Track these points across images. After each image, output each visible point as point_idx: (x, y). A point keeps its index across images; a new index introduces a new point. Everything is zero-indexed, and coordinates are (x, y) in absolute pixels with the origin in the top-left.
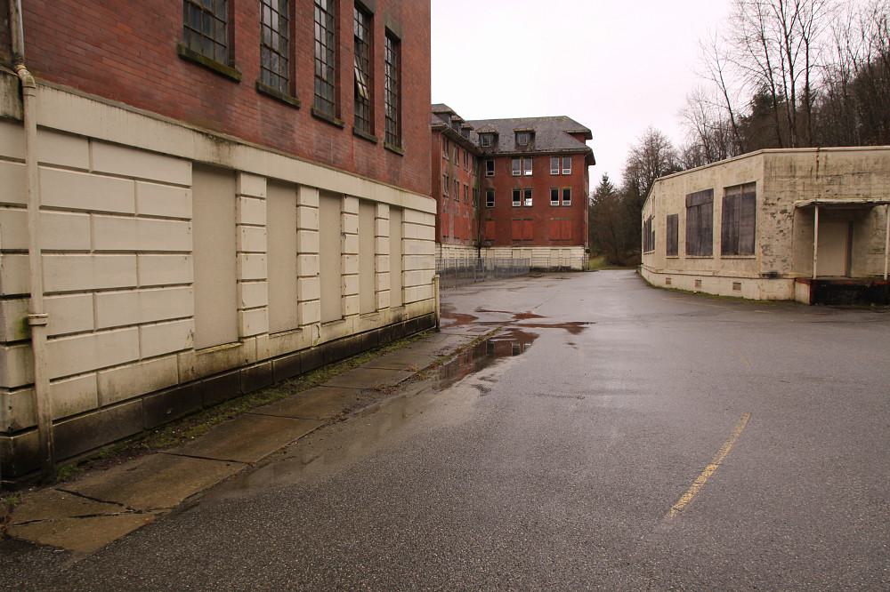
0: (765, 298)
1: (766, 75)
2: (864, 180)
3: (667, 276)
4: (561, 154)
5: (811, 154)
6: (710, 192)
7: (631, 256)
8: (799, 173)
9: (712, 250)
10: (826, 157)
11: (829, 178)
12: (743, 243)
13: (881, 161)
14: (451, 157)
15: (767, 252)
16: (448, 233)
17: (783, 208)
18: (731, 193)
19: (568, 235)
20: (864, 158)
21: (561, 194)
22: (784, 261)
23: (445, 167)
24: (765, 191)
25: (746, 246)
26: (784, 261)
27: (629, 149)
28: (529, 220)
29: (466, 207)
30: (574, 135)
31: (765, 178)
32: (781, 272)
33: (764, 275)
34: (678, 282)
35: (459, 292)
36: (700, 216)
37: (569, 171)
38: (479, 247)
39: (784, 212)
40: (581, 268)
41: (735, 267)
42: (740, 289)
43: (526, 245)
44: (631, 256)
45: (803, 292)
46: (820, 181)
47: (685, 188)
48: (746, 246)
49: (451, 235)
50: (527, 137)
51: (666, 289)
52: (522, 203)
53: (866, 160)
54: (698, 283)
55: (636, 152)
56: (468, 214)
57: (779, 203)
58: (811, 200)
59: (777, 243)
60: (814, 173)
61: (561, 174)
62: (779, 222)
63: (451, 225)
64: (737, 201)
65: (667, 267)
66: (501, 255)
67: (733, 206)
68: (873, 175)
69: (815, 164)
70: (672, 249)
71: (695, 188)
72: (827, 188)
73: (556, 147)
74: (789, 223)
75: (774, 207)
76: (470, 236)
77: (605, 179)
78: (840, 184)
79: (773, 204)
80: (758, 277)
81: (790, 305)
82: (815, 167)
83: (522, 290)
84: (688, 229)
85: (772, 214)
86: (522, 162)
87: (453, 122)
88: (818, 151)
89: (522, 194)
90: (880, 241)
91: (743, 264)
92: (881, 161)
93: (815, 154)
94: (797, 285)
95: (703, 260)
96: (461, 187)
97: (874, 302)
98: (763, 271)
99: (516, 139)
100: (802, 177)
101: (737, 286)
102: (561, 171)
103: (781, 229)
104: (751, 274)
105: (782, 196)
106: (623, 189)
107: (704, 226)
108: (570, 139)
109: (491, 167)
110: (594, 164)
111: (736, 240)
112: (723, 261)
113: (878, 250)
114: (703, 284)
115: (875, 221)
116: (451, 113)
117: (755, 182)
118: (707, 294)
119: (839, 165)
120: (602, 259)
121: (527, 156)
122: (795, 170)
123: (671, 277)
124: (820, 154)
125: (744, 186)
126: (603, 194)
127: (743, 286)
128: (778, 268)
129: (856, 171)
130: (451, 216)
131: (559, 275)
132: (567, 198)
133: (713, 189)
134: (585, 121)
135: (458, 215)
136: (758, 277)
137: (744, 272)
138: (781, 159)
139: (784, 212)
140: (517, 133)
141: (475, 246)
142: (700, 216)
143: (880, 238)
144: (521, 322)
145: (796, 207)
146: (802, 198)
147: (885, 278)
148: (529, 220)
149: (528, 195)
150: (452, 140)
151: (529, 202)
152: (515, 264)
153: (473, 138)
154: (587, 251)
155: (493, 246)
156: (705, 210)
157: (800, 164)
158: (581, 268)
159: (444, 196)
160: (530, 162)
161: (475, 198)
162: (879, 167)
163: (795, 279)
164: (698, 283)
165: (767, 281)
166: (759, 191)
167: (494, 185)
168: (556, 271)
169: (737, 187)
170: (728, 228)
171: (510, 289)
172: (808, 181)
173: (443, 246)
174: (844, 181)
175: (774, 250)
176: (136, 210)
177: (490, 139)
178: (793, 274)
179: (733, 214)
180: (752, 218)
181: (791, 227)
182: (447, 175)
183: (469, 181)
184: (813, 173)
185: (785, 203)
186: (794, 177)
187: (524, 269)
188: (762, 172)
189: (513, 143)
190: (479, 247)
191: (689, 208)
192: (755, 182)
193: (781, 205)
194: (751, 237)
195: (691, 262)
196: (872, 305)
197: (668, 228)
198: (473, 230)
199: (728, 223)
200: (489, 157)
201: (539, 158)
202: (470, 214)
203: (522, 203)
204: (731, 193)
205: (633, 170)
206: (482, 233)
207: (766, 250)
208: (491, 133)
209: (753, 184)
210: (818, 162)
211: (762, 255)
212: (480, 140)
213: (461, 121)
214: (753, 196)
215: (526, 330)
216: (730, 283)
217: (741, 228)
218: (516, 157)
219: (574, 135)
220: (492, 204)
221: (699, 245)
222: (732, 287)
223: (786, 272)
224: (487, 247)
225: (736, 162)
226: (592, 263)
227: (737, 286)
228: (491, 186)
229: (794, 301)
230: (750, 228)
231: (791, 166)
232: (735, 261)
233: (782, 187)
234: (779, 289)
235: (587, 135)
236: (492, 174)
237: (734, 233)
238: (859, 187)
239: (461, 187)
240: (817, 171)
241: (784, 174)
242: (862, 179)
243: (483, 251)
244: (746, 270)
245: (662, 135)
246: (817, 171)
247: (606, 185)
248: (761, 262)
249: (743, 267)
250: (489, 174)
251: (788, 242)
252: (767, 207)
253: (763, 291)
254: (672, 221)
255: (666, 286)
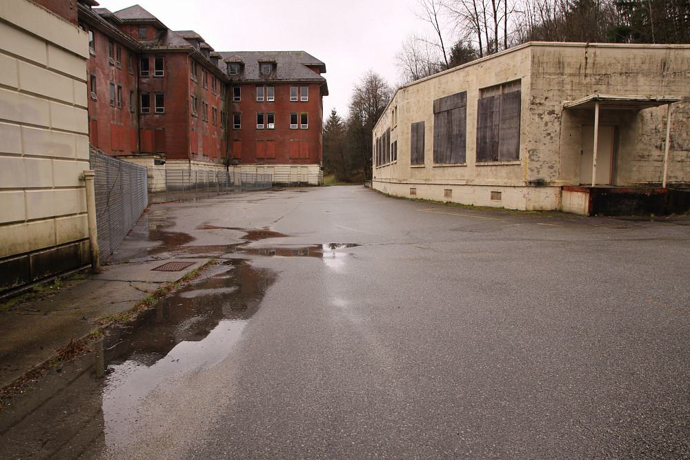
0: (531, 208)
1: (474, 20)
2: (631, 81)
3: (412, 186)
4: (300, 83)
5: (580, 49)
6: (463, 95)
7: (356, 174)
8: (568, 70)
9: (465, 157)
10: (595, 54)
11: (598, 77)
12: (503, 148)
13: (647, 61)
14: (199, 80)
15: (534, 158)
16: (197, 150)
17: (551, 109)
18: (488, 95)
19: (306, 154)
20: (632, 56)
21: (299, 119)
22: (551, 167)
23: (193, 90)
24: (532, 89)
25: (508, 151)
26: (551, 167)
27: (367, 70)
28: (271, 141)
29: (214, 127)
30: (311, 67)
31: (533, 74)
32: (548, 180)
33: (530, 183)
34: (423, 192)
35: (201, 204)
36: (450, 122)
37: (306, 99)
38: (227, 164)
39: (551, 113)
40: (317, 183)
41: (493, 175)
42: (500, 199)
43: (269, 163)
44: (356, 174)
45: (578, 202)
46: (588, 79)
47: (433, 93)
48: (508, 151)
49: (200, 153)
50: (270, 67)
51: (412, 200)
52: (265, 126)
53: (634, 58)
54: (448, 193)
55: (360, 90)
56: (217, 135)
57: (547, 103)
58: (591, 97)
59: (543, 147)
60: (582, 71)
61: (299, 101)
62: (546, 124)
63: (200, 144)
64: (496, 103)
65: (411, 177)
66: (248, 171)
67: (491, 108)
68: (640, 75)
69: (584, 61)
70: (418, 158)
71: (444, 92)
72: (595, 88)
73: (295, 76)
74: (556, 126)
75: (541, 107)
76: (219, 154)
77: (334, 113)
78: (608, 84)
79: (540, 104)
80: (524, 185)
81: (559, 216)
82: (583, 64)
83: (262, 201)
84: (436, 137)
85: (540, 115)
86: (265, 89)
87: (202, 49)
88: (587, 47)
89: (266, 118)
90: (644, 147)
91: (504, 171)
92: (647, 61)
93: (584, 50)
94: (564, 193)
95: (453, 169)
96: (209, 109)
97: (653, 213)
98: (529, 179)
99: (260, 69)
100: (571, 75)
101: (496, 195)
102: (299, 98)
103: (548, 132)
104: (514, 182)
105: (550, 95)
106: (349, 120)
107: (455, 132)
108: (307, 70)
109: (237, 93)
110: (327, 94)
111: (495, 145)
112: (479, 169)
113: (643, 157)
114: (454, 193)
115: (640, 125)
116: (200, 40)
117: (520, 80)
118: (459, 205)
119: (608, 63)
120: (333, 177)
121: (270, 84)
122: (563, 68)
123: (416, 186)
124: (591, 50)
125: (504, 85)
126: (332, 125)
127: (503, 195)
128: (544, 175)
129: (624, 71)
130: (200, 135)
131: (299, 189)
132: (304, 121)
133: (466, 92)
134: (321, 57)
135: (207, 134)
136: (524, 185)
137: (506, 180)
138: (549, 53)
139: (551, 113)
140: (261, 63)
141: (223, 164)
142: (450, 122)
143: (646, 144)
144: (254, 244)
145: (565, 108)
146: (570, 98)
147: (664, 186)
148: (271, 141)
149: (271, 120)
150: (200, 64)
151: (272, 126)
152: (259, 180)
153: (222, 65)
154: (322, 169)
155: (240, 163)
156: (456, 115)
157: (569, 60)
158: (317, 183)
159: (193, 116)
160: (271, 90)
161: (223, 120)
162: (645, 67)
163: (562, 188)
164: (448, 193)
165: (533, 189)
166: (525, 89)
167: (241, 109)
168: (295, 186)
169: (497, 87)
170: (485, 132)
171: (250, 201)
172: (576, 80)
173: (192, 162)
174: (613, 80)
175: (541, 156)
176: (23, 151)
177: (236, 68)
178: (560, 182)
179: (491, 116)
180: (515, 120)
181: (558, 130)
182: (195, 96)
183: (217, 105)
184: (580, 72)
185: (552, 103)
186: (562, 74)
187: (267, 184)
188: (529, 67)
189: (257, 72)
190: (227, 164)
191: (437, 114)
192: (520, 80)
193: (549, 105)
194: (514, 141)
195: (439, 171)
196: (652, 215)
197: (412, 136)
198: (221, 149)
199: (486, 127)
200: (236, 84)
201: (281, 86)
202: (219, 134)
203: (265, 126)
204: (488, 95)
205: (358, 104)
206: (230, 152)
207: (533, 155)
208: (238, 63)
209: (519, 81)
210: (586, 58)
211: (528, 161)
212: (227, 68)
213: (209, 49)
214: (518, 96)
215: (257, 262)
216: (441, 190)
217: (501, 133)
218: (259, 84)
219: (311, 67)
220: (239, 127)
221: (449, 153)
222: (490, 198)
223: (554, 179)
224: (235, 165)
225: (495, 60)
226: (327, 180)
227: (496, 195)
228: (238, 110)
229: (561, 211)
230: (514, 131)
231: (559, 63)
232: (494, 168)
233: (550, 85)
234: (546, 199)
235: (321, 68)
236: (239, 99)
237: (492, 137)
238: (625, 88)
239: (209, 109)
240: (586, 68)
241: (552, 70)
242: (629, 79)
243: (231, 169)
244: (509, 178)
245: (380, 77)
246: (586, 68)
247: (334, 117)
248: (525, 168)
249: (505, 175)
250: (236, 99)
251: (555, 147)
252: (535, 107)
253: (530, 200)
254: (418, 129)
255: (410, 196)
